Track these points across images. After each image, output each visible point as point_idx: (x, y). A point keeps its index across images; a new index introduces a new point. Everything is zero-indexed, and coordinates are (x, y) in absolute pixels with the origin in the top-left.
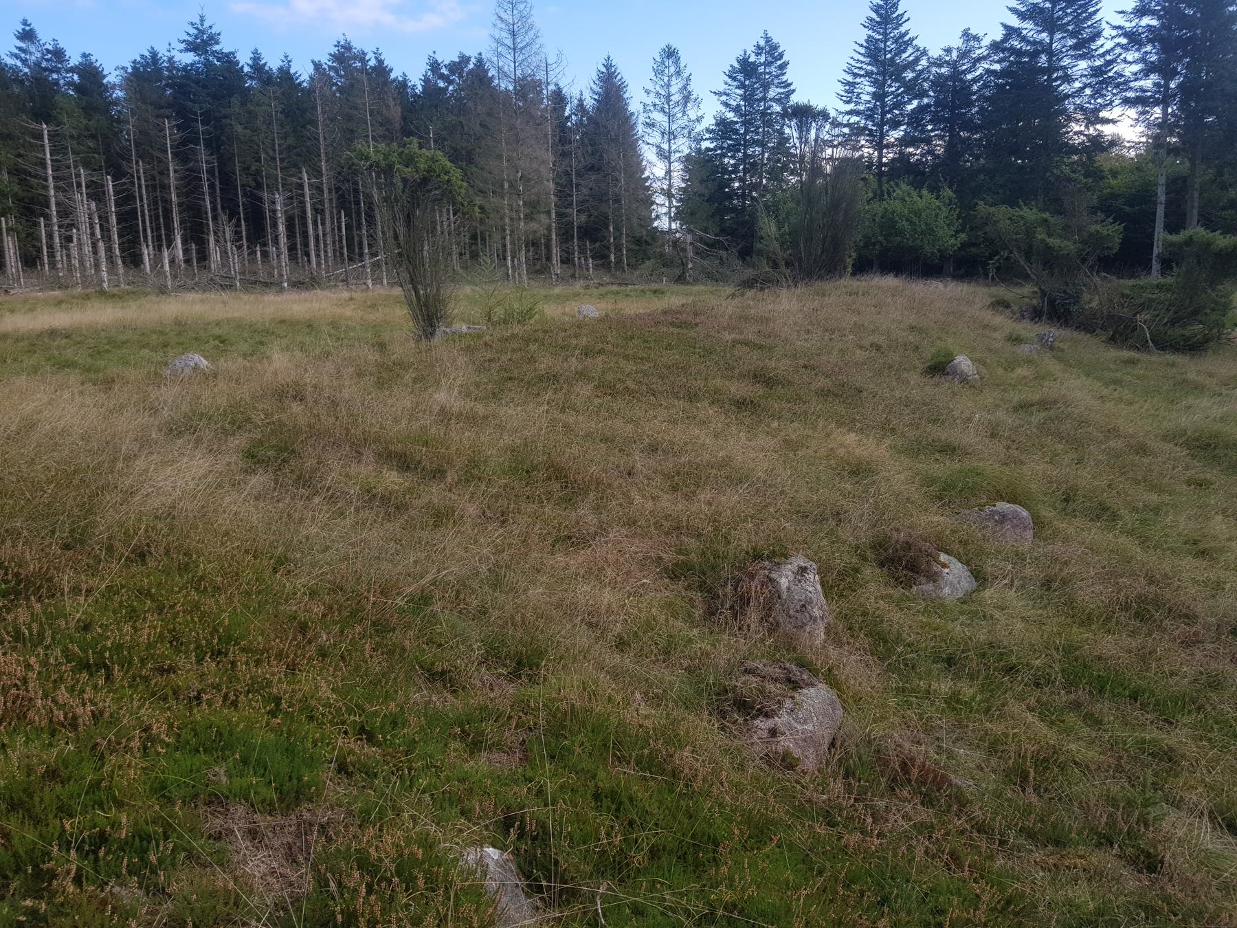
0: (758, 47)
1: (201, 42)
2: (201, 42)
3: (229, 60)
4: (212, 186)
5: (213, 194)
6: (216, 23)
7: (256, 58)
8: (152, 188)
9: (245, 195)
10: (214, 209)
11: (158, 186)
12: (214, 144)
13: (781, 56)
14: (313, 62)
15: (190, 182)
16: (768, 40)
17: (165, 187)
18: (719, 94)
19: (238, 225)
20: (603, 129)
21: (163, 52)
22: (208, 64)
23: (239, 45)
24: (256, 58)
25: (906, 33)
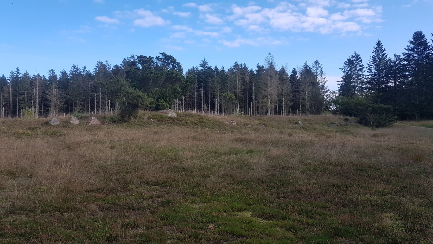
0: (352, 56)
1: (236, 65)
2: (204, 65)
3: (210, 68)
4: (204, 98)
5: (203, 99)
6: (207, 60)
7: (216, 67)
8: (190, 98)
9: (211, 99)
10: (204, 103)
11: (192, 98)
12: (205, 88)
13: (360, 58)
14: (18, 68)
15: (199, 96)
16: (356, 54)
17: (194, 98)
18: (342, 69)
19: (208, 106)
20: (309, 76)
21: (195, 67)
22: (205, 69)
23: (212, 64)
24: (216, 67)
25: (385, 54)
